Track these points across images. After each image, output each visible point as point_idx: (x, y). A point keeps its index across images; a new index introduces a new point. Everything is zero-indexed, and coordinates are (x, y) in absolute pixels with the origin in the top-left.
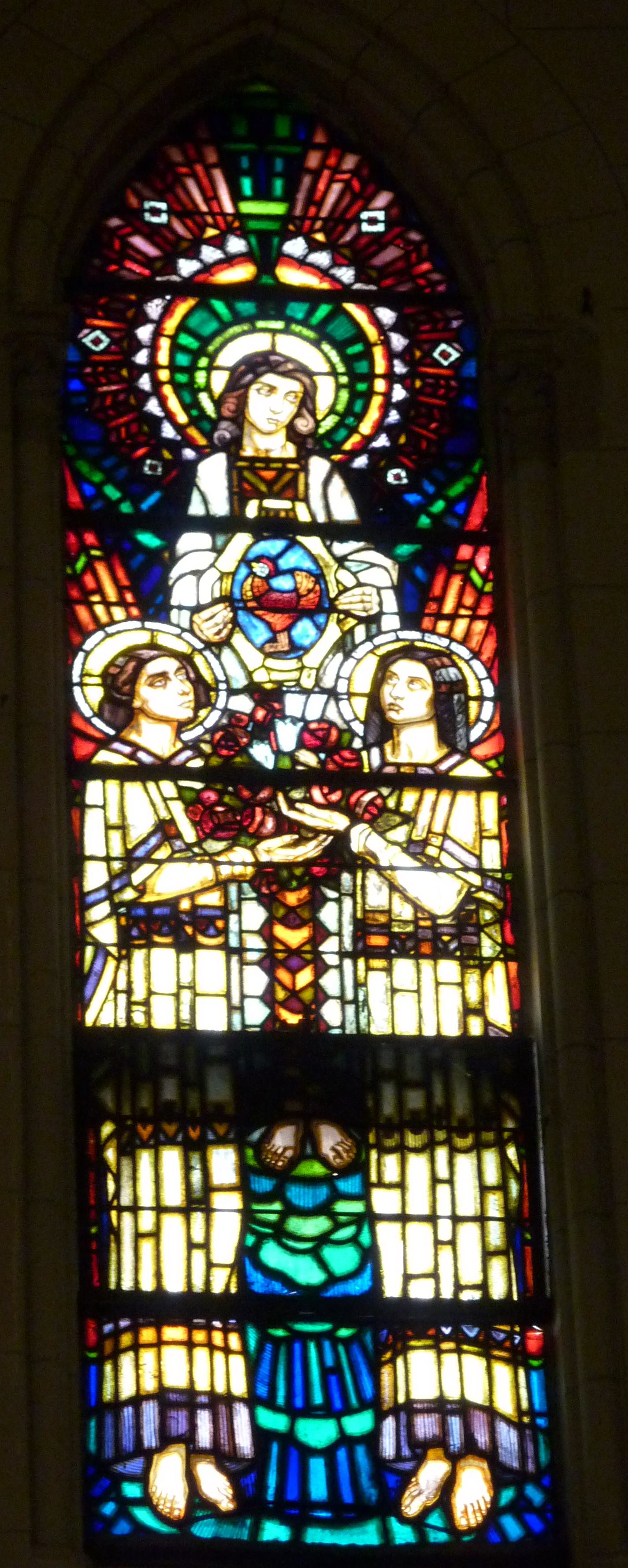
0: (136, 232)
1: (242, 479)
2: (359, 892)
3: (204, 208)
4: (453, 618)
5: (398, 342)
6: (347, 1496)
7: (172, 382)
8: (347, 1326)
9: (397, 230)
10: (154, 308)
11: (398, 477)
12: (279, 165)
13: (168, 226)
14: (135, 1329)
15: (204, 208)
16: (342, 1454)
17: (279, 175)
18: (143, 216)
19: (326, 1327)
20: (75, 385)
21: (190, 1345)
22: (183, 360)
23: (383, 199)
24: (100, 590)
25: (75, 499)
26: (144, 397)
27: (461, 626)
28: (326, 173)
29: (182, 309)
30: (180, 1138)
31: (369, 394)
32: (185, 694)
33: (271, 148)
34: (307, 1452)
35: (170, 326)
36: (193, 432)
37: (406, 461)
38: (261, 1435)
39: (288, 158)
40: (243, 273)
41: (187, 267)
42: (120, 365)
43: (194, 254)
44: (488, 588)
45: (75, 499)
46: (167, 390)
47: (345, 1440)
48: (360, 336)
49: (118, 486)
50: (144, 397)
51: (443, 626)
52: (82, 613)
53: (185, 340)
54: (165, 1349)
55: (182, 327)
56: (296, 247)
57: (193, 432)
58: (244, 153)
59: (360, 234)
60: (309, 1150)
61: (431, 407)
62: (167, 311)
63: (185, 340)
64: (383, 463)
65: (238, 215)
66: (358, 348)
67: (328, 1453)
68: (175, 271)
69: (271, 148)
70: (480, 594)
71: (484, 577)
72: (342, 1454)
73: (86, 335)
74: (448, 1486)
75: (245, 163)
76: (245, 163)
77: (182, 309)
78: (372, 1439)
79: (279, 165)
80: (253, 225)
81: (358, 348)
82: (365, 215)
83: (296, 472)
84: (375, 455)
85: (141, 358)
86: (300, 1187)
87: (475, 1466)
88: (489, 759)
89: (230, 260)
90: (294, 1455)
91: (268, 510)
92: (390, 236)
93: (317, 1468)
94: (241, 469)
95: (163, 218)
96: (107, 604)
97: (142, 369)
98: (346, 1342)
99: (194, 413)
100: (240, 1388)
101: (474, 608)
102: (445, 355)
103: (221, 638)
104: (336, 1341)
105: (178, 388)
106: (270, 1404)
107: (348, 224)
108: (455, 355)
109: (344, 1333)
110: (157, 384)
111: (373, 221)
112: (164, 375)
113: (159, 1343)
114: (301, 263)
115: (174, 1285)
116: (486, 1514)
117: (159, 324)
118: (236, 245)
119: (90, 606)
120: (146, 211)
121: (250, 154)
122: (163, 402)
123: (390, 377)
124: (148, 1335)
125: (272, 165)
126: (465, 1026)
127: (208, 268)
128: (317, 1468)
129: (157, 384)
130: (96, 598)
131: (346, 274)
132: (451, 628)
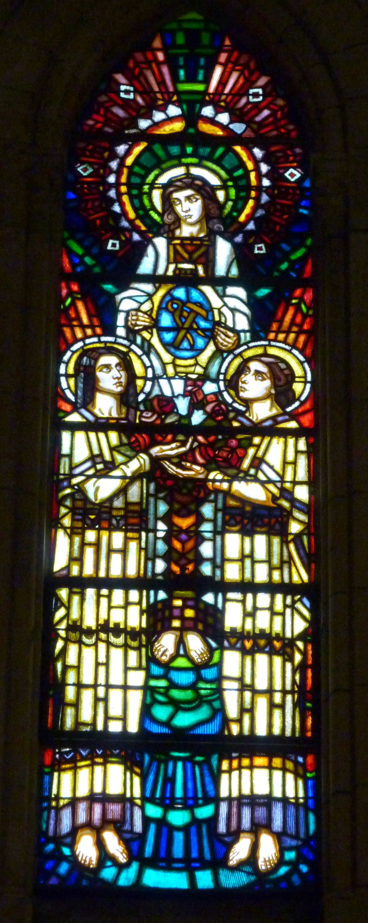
0: (116, 104)
1: (176, 252)
2: (145, 496)
3: (156, 89)
4: (288, 332)
5: (264, 168)
6: (194, 854)
7: (128, 193)
8: (200, 755)
9: (269, 99)
10: (121, 149)
11: (114, 245)
12: (202, 61)
13: (134, 100)
14: (240, 758)
15: (156, 89)
16: (193, 830)
17: (181, 67)
18: (119, 94)
19: (187, 755)
20: (71, 196)
21: (270, 767)
22: (135, 180)
23: (263, 81)
24: (78, 318)
25: (67, 265)
26: (112, 201)
27: (292, 336)
28: (230, 66)
29: (137, 150)
30: (239, 645)
31: (248, 198)
32: (244, 382)
33: (198, 51)
34: (172, 828)
35: (129, 161)
36: (138, 222)
37: (266, 239)
38: (146, 820)
39: (207, 57)
40: (178, 126)
41: (144, 124)
42: (98, 184)
43: (149, 116)
44: (311, 312)
45: (67, 265)
46: (125, 199)
47: (195, 822)
48: (242, 164)
49: (93, 257)
50: (112, 201)
51: (281, 336)
52: (67, 332)
53: (137, 169)
54: (256, 771)
55: (136, 162)
56: (208, 111)
57: (138, 222)
58: (181, 55)
59: (248, 103)
60: (182, 652)
61: (283, 205)
62: (128, 153)
63: (137, 169)
64: (251, 241)
65: (177, 92)
66: (240, 172)
67: (185, 829)
68: (136, 126)
69: (198, 51)
70: (305, 316)
71: (308, 308)
72: (193, 830)
73: (79, 166)
74: (255, 847)
75: (181, 62)
76: (181, 62)
77: (137, 150)
78: (214, 820)
79: (202, 61)
80: (184, 97)
81: (240, 172)
82: (251, 91)
83: (208, 246)
84: (248, 234)
85: (112, 179)
86: (182, 673)
87: (80, 836)
88: (175, 413)
89: (170, 120)
90: (165, 830)
91: (181, 269)
92: (264, 104)
93: (179, 837)
94: (175, 245)
95: (131, 96)
96: (83, 327)
97: (110, 186)
98: (199, 764)
99: (141, 212)
100: (137, 793)
101: (300, 326)
102: (292, 175)
103: (222, 348)
104: (194, 763)
105: (131, 198)
106: (152, 800)
107: (241, 96)
108: (298, 175)
109: (198, 759)
110: (119, 194)
111: (256, 95)
112: (124, 189)
113: (251, 767)
114: (212, 121)
115: (261, 731)
116: (276, 863)
117: (123, 159)
118: (173, 110)
119: (72, 327)
120: (250, 95)
121: (185, 56)
122: (122, 205)
123: (118, 184)
124: (246, 762)
125: (198, 61)
126: (270, 575)
127: (157, 125)
128: (179, 837)
129: (119, 194)
130: (75, 323)
131: (239, 128)
132: (286, 338)
